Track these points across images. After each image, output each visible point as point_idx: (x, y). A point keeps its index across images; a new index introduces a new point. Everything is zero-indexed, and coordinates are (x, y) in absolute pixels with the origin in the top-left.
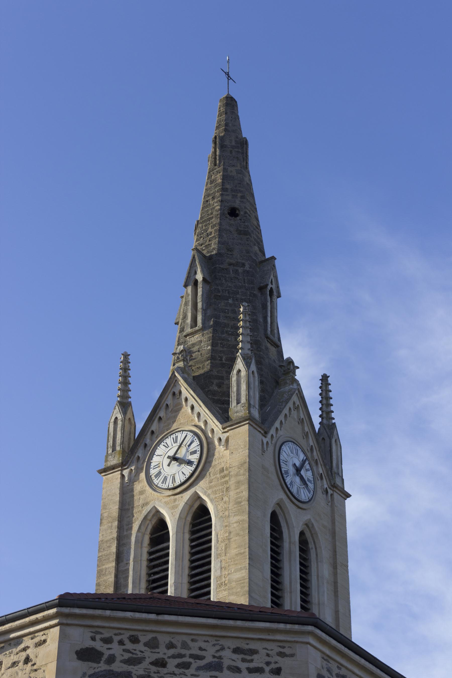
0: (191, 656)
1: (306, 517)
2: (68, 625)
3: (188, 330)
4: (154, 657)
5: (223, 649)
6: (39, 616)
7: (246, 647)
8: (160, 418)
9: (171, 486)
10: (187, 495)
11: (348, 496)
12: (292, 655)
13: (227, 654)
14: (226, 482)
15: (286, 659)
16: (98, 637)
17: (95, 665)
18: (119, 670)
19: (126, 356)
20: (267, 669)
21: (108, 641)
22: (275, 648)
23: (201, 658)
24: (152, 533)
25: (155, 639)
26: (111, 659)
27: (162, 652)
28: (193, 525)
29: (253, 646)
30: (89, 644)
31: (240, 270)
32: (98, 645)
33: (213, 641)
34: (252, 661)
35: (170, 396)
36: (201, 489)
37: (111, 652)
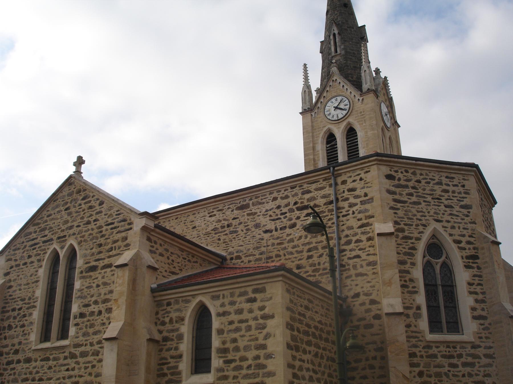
0: (430, 179)
1: (390, 134)
2: (380, 164)
3: (333, 54)
4: (416, 179)
5: (441, 176)
6: (366, 160)
7: (450, 176)
8: (327, 91)
9: (337, 119)
10: (345, 123)
11: (399, 126)
12: (468, 180)
13: (443, 178)
14: (364, 117)
15: (466, 181)
16: (392, 170)
17: (393, 181)
18: (403, 184)
19: (305, 65)
20: (460, 185)
21: (396, 172)
22: (461, 177)
23: (434, 180)
24: (327, 139)
25: (415, 171)
26: (399, 179)
27: (419, 177)
28: (347, 135)
29: (453, 175)
30: (389, 172)
31: (352, 30)
32: (393, 173)
33: (437, 173)
34: (453, 182)
35: (331, 81)
36: (351, 120)
37: (399, 176)
